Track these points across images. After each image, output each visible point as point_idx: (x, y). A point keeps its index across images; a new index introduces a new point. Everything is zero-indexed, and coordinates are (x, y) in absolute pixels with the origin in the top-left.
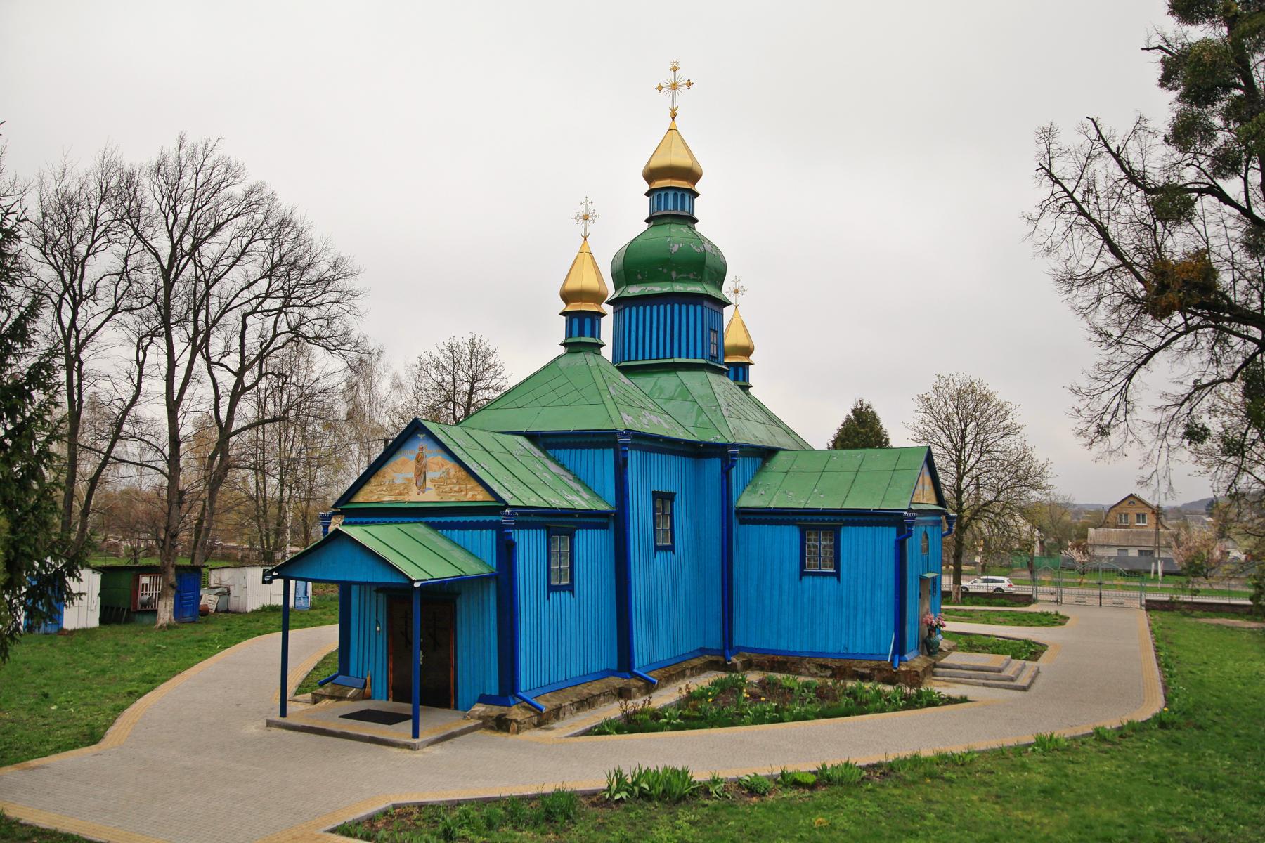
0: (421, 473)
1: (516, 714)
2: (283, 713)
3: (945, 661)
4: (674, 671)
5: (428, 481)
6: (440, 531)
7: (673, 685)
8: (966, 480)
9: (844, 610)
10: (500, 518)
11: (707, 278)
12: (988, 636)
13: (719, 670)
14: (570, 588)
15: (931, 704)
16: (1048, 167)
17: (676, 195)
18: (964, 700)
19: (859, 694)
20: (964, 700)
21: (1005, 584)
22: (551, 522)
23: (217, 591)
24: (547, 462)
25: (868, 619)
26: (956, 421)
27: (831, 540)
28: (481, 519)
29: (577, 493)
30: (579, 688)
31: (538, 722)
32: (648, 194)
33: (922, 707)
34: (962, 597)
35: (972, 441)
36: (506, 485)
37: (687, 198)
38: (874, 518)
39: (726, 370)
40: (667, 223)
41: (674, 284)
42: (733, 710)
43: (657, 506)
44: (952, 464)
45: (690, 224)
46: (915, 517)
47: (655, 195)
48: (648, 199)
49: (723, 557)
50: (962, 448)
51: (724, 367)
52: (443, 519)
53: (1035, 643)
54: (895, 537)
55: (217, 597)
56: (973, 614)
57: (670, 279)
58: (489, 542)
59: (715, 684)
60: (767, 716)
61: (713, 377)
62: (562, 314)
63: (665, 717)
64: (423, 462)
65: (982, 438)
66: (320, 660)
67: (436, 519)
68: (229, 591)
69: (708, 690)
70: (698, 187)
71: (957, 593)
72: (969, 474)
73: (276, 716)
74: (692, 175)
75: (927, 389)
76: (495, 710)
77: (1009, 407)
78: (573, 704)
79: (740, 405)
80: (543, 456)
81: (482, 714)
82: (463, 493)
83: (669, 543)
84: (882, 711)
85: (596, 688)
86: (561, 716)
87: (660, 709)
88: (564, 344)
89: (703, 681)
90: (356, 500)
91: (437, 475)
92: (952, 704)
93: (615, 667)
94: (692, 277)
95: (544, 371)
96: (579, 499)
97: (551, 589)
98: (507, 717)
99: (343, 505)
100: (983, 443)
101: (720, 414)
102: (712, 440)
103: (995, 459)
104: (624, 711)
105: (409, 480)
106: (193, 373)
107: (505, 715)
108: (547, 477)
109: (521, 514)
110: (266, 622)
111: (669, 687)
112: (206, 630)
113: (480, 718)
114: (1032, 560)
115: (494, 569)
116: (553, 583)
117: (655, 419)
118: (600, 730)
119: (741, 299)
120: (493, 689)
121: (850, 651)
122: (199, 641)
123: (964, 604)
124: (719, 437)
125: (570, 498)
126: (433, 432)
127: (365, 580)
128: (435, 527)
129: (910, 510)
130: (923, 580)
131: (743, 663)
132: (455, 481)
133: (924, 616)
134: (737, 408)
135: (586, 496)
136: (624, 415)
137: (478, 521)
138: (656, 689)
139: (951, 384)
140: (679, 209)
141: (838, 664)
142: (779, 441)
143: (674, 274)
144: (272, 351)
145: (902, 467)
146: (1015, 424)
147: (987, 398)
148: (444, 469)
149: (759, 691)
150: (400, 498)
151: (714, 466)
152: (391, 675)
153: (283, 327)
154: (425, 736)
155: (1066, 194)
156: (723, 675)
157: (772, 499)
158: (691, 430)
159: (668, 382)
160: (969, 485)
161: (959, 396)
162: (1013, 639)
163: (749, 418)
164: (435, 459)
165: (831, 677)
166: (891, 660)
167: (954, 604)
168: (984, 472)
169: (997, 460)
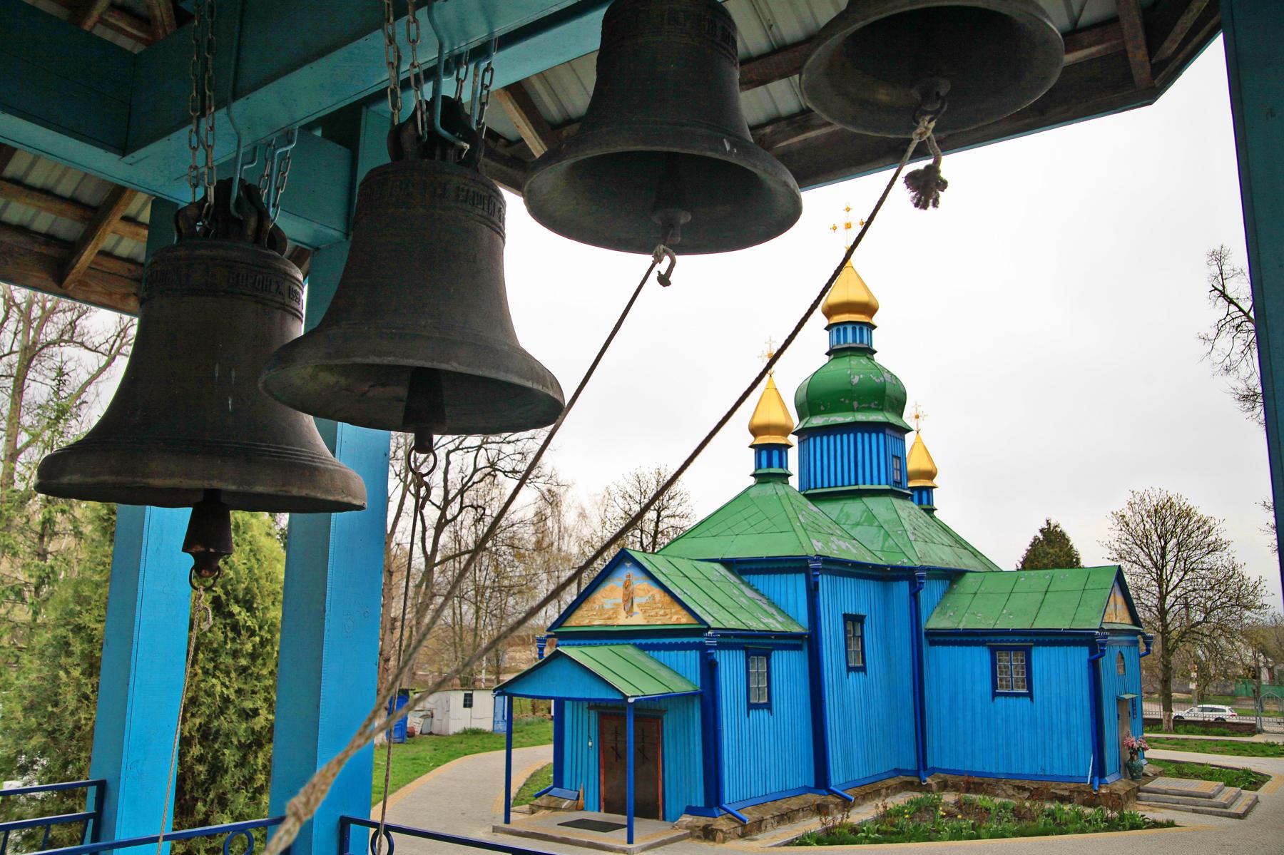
0: (629, 599)
1: (721, 824)
2: (507, 820)
3: (1150, 785)
4: (870, 790)
5: (635, 606)
6: (647, 652)
7: (869, 803)
8: (1170, 600)
9: (1039, 731)
10: (703, 640)
11: (887, 406)
12: (1203, 764)
13: (914, 790)
14: (768, 706)
15: (1135, 827)
16: (1221, 288)
17: (854, 329)
18: (1170, 824)
19: (1058, 816)
20: (1170, 824)
21: (1227, 713)
22: (749, 644)
23: (422, 713)
24: (742, 586)
25: (1064, 741)
26: (1155, 538)
27: (1022, 661)
28: (685, 640)
29: (772, 616)
30: (779, 802)
31: (742, 833)
32: (827, 328)
33: (1125, 829)
34: (1174, 726)
35: (1174, 559)
36: (707, 609)
37: (865, 331)
38: (1065, 638)
39: (908, 495)
40: (847, 356)
41: (856, 414)
42: (930, 826)
43: (848, 628)
44: (1154, 583)
45: (869, 356)
46: (1108, 636)
47: (835, 329)
48: (827, 333)
49: (914, 692)
50: (1163, 566)
51: (908, 492)
52: (649, 641)
53: (1256, 773)
54: (1088, 657)
55: (422, 720)
56: (1187, 743)
57: (853, 410)
58: (693, 662)
59: (911, 802)
60: (964, 833)
61: (898, 503)
62: (751, 447)
63: (863, 831)
64: (630, 588)
65: (1185, 555)
66: (528, 777)
67: (643, 641)
68: (432, 714)
69: (904, 808)
70: (875, 320)
71: (1169, 721)
72: (1173, 594)
73: (501, 824)
74: (869, 309)
75: (1121, 506)
76: (702, 821)
77: (1212, 522)
78: (773, 818)
79: (926, 529)
80: (738, 582)
81: (690, 824)
82: (668, 617)
83: (861, 665)
84: (1082, 831)
85: (794, 803)
86: (763, 828)
87: (859, 825)
88: (754, 475)
89: (900, 800)
90: (567, 624)
91: (643, 600)
92: (1157, 827)
93: (812, 785)
94: (873, 406)
95: (736, 501)
96: (774, 622)
97: (751, 707)
98: (714, 827)
99: (557, 628)
100: (1186, 560)
101: (906, 537)
102: (899, 563)
103: (1201, 578)
104: (823, 824)
105: (618, 605)
106: (404, 508)
107: (711, 825)
108: (743, 601)
109: (723, 636)
110: (470, 744)
111: (865, 805)
112: (416, 750)
113: (687, 828)
114: (1258, 687)
115: (698, 687)
116: (752, 701)
117: (843, 544)
118: (801, 841)
119: (922, 424)
120: (699, 802)
121: (1048, 773)
122: (414, 759)
123: (1177, 732)
124: (906, 560)
125: (765, 621)
126: (639, 560)
127: (583, 697)
128: (643, 648)
129: (1101, 629)
130: (1120, 701)
131: (938, 783)
132: (660, 605)
133: (1124, 739)
134: (923, 531)
135: (780, 619)
136: (814, 542)
137: (658, 643)
138: (853, 807)
139: (1147, 500)
140: (858, 342)
141: (1035, 786)
142: (967, 562)
143: (855, 404)
144: (472, 485)
145: (1092, 587)
146: (1221, 540)
147: (1188, 514)
148: (649, 595)
149: (955, 810)
150: (609, 622)
151: (903, 588)
152: (602, 788)
153: (482, 462)
154: (638, 843)
155: (1241, 313)
156: (918, 795)
157: (961, 621)
158: (878, 554)
159: (854, 508)
160: (1173, 605)
161: (1156, 511)
162: (1231, 768)
163: (935, 541)
164: (642, 586)
165: (1028, 799)
166: (1091, 783)
167: (1166, 732)
168: (1189, 591)
169: (1203, 578)
